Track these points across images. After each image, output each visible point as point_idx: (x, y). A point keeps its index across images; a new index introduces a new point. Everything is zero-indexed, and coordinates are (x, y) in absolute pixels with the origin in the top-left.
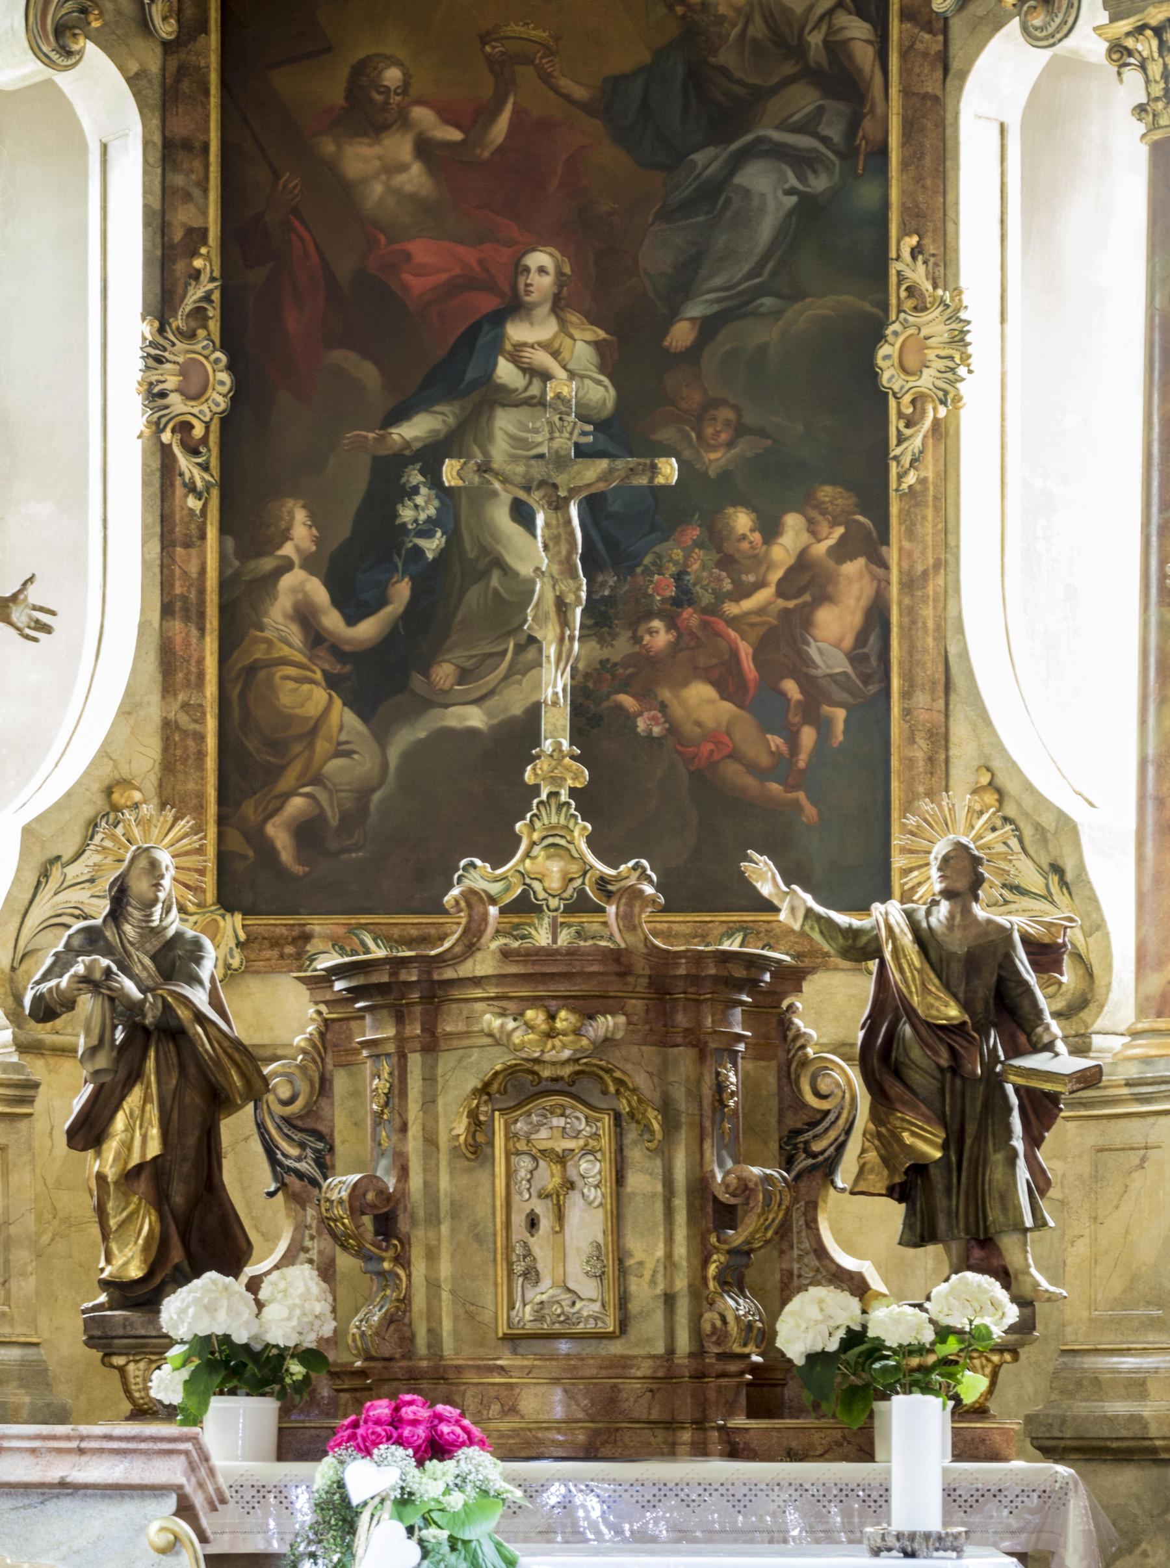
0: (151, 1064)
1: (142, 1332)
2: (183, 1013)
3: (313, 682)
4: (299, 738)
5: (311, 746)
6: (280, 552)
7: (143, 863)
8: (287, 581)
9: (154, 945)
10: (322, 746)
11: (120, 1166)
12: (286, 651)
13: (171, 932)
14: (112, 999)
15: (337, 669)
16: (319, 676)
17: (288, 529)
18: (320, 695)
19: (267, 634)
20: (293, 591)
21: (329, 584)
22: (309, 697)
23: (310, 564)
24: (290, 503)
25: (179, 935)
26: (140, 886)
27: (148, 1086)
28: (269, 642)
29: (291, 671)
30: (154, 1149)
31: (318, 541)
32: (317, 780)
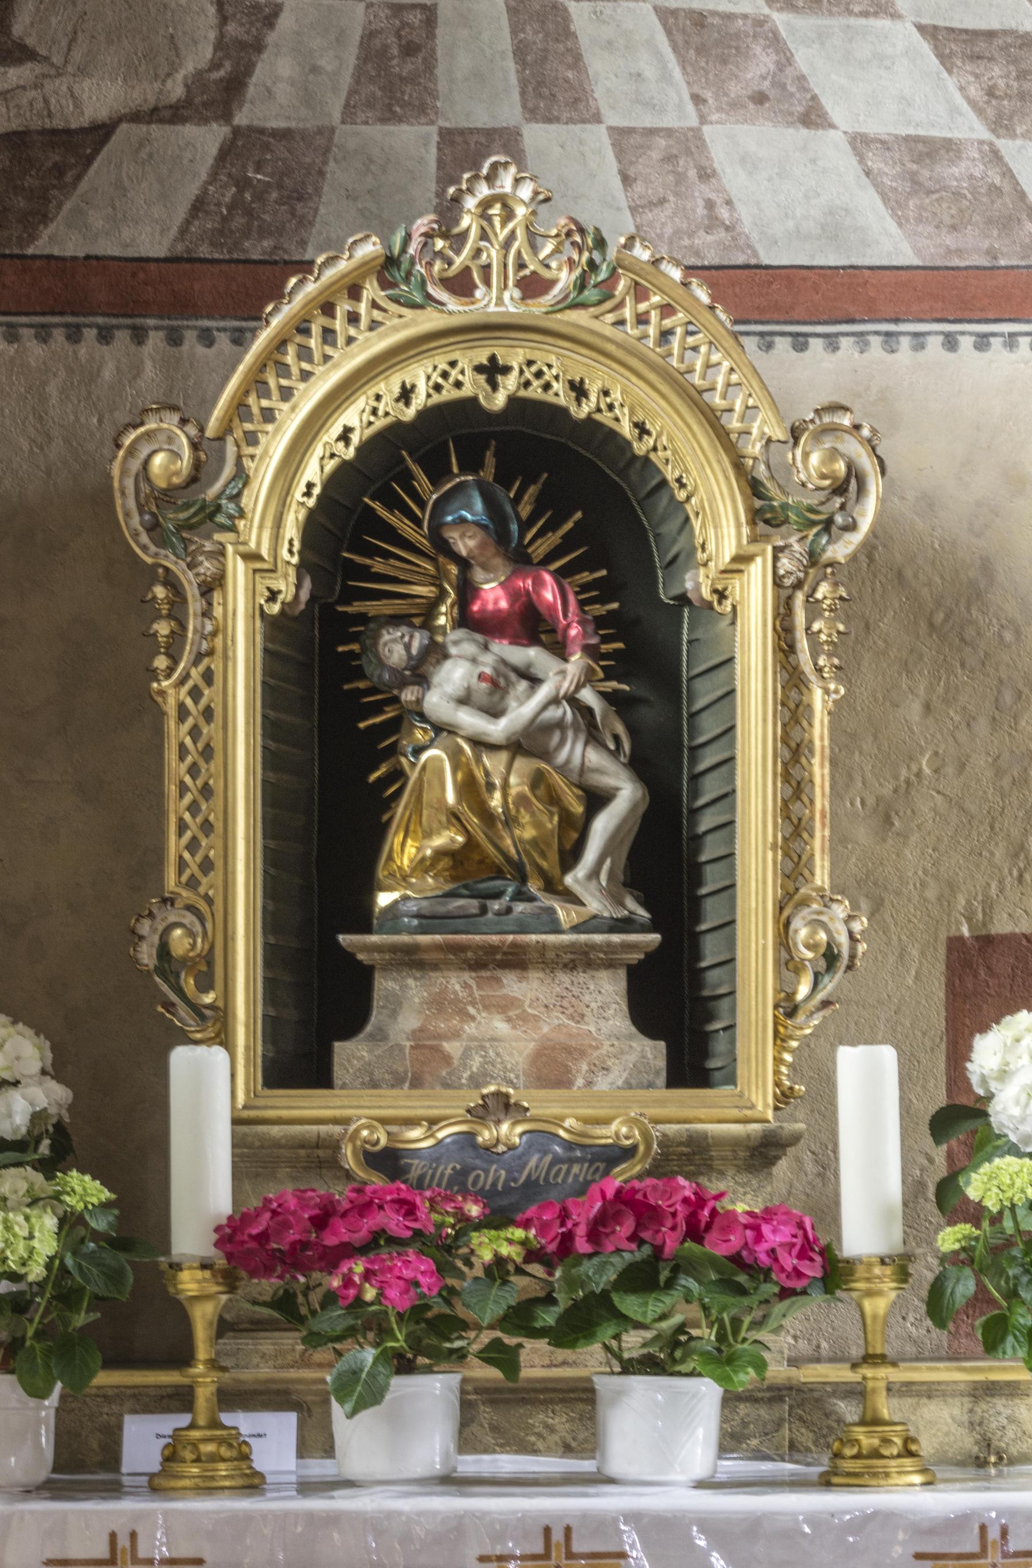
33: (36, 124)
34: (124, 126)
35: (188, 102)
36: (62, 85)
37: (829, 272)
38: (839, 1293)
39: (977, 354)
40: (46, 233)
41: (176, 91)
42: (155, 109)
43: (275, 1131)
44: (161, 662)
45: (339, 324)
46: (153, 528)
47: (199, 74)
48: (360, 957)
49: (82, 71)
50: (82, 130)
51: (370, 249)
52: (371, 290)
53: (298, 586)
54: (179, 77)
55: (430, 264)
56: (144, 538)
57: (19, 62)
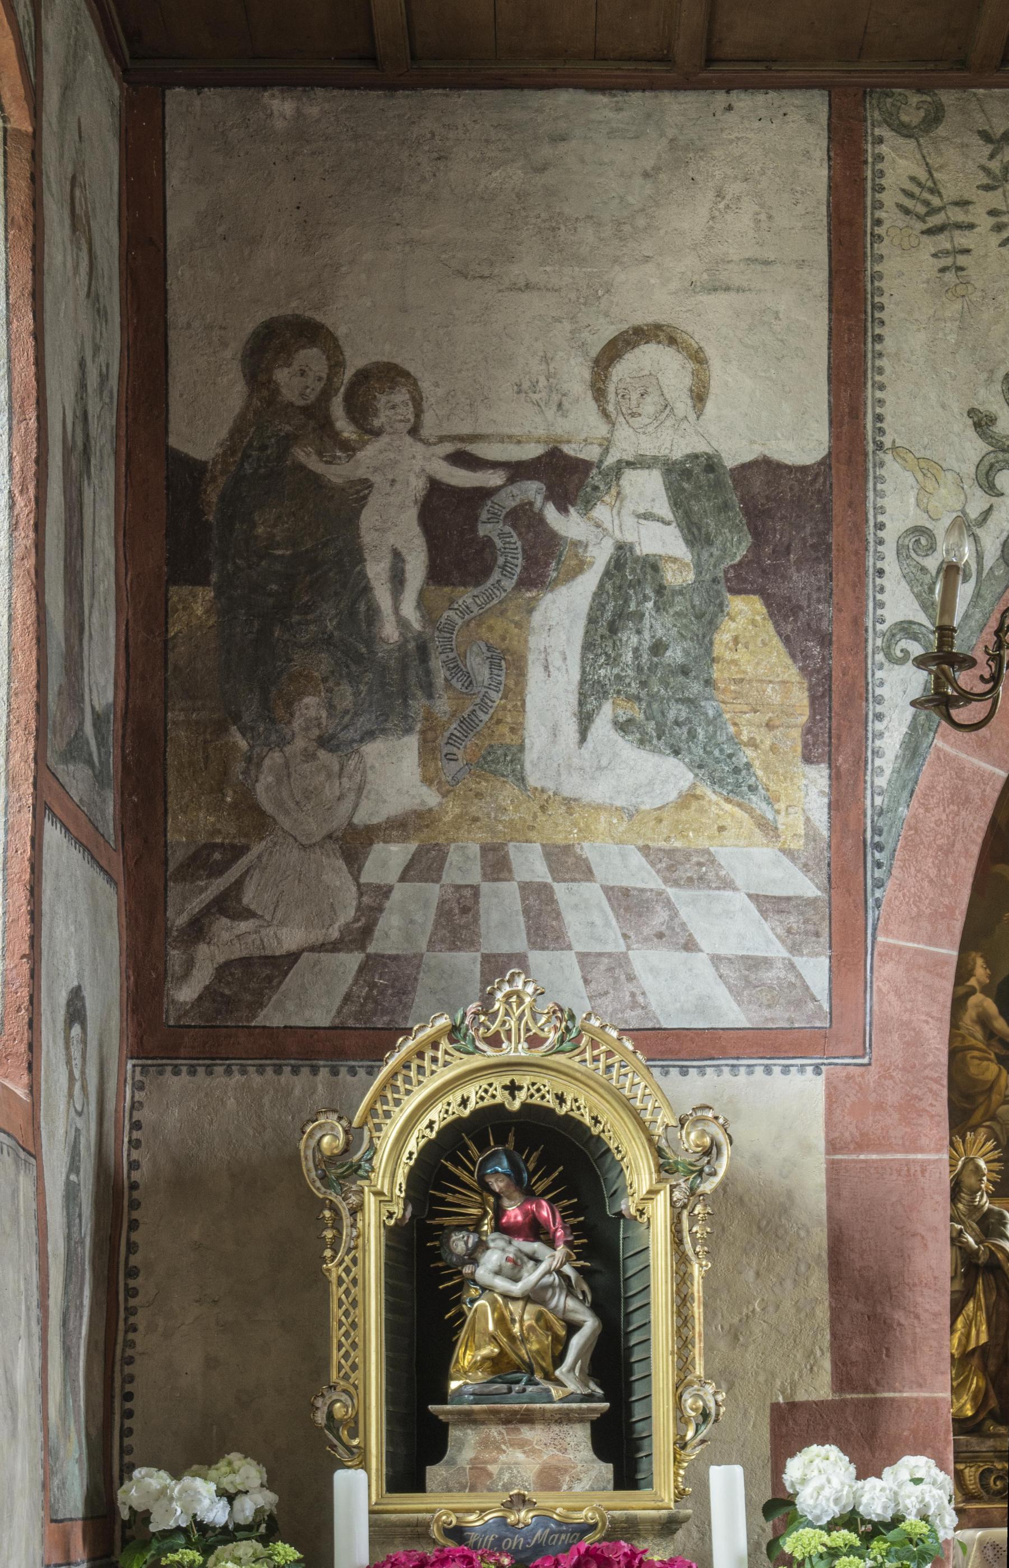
0: (980, 1287)
1: (977, 1449)
2: (1000, 1256)
3: (989, 1060)
4: (982, 1093)
5: (989, 1098)
6: (969, 983)
7: (971, 1167)
8: (973, 1000)
9: (977, 1216)
10: (996, 1098)
11: (961, 1349)
12: (973, 1042)
13: (986, 1208)
14: (960, 1248)
15: (1003, 1052)
16: (993, 1056)
17: (973, 969)
18: (994, 1068)
19: (961, 1032)
20: (977, 1006)
21: (997, 1002)
22: (987, 1069)
23: (985, 990)
24: (973, 954)
25: (990, 1210)
26: (970, 1180)
27: (979, 1300)
28: (964, 1037)
29: (976, 1053)
30: (984, 1339)
31: (990, 977)
32: (993, 1118)
33: (257, 953)
34: (305, 954)
41: (335, 934)
42: (323, 945)
44: (328, 1253)
45: (426, 1063)
46: (323, 1178)
49: (282, 924)
50: (282, 956)
52: (444, 1044)
53: (405, 1210)
54: (336, 926)
56: (318, 1184)
57: (246, 918)
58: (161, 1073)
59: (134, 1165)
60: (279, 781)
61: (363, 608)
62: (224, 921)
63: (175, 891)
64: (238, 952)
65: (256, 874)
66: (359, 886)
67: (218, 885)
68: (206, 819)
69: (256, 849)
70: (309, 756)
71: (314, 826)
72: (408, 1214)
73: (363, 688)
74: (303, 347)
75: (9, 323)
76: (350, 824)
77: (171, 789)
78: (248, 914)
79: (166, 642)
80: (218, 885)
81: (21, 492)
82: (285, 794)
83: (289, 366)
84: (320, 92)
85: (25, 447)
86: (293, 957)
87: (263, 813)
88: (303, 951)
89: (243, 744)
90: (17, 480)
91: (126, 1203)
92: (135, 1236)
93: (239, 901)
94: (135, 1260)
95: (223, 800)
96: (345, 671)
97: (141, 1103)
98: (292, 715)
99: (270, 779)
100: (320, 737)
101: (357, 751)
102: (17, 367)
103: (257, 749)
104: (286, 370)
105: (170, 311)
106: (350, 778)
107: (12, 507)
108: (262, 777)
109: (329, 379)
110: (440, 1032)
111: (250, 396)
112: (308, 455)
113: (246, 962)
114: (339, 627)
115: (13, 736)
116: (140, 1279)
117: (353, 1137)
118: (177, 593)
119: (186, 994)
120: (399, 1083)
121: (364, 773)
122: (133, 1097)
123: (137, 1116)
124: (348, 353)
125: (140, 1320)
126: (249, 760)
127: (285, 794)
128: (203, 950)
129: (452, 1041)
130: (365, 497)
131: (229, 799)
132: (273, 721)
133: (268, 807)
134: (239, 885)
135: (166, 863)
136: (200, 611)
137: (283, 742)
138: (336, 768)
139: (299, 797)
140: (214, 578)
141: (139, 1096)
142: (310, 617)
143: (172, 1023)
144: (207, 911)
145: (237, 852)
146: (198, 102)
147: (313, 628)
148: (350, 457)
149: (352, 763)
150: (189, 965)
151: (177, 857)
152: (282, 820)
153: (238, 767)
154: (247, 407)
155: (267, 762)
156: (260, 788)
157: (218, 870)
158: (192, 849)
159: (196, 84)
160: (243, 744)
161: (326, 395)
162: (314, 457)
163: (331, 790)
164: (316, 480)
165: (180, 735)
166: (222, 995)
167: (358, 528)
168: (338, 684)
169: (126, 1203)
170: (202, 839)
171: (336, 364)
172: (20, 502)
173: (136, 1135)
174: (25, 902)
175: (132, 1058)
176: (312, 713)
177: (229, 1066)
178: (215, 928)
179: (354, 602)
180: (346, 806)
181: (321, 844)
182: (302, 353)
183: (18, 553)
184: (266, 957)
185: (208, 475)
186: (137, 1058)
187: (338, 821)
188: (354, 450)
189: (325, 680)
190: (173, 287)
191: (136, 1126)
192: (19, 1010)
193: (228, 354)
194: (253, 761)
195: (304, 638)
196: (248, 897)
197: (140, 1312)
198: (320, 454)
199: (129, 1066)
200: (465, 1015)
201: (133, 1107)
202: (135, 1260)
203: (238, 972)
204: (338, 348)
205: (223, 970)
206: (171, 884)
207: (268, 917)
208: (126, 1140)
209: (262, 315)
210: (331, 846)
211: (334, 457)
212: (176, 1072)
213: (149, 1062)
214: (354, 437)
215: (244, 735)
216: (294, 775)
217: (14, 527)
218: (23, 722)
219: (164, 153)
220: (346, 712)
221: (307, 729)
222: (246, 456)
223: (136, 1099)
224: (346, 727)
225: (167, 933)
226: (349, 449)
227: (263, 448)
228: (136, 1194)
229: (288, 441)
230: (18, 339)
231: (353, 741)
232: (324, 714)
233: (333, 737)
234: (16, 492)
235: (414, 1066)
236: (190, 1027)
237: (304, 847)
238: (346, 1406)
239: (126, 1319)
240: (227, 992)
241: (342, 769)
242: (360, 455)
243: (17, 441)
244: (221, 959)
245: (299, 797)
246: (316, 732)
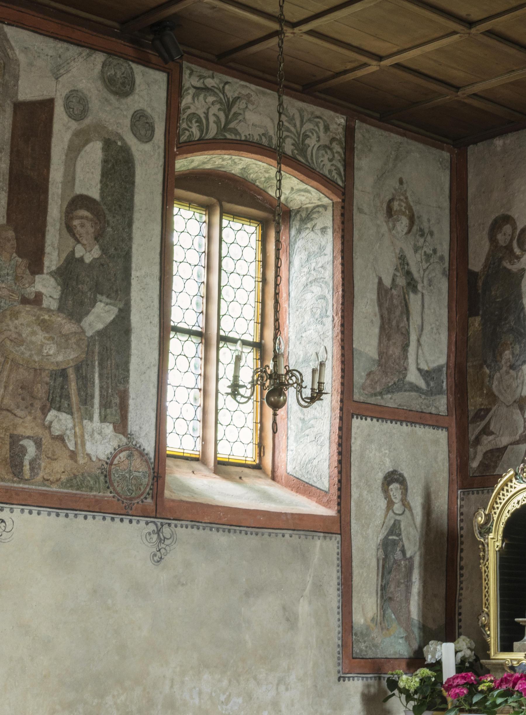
33: (494, 447)
34: (509, 446)
35: (520, 440)
36: (499, 438)
37: (33, 504)
38: (407, 688)
39: (39, 516)
40: (497, 469)
41: (518, 438)
42: (514, 442)
43: (494, 661)
44: (482, 561)
45: (509, 488)
46: (480, 533)
47: (521, 434)
48: (521, 623)
49: (502, 436)
50: (502, 448)
51: (512, 472)
52: (514, 480)
53: (502, 544)
54: (518, 435)
55: (523, 474)
56: (479, 535)
57: (491, 435)
58: (469, 494)
59: (462, 528)
60: (499, 383)
61: (522, 315)
62: (485, 437)
63: (471, 427)
64: (489, 447)
65: (494, 418)
66: (524, 419)
67: (483, 423)
68: (479, 400)
69: (494, 408)
70: (507, 373)
71: (510, 398)
72: (504, 545)
73: (522, 345)
74: (505, 225)
75: (333, 262)
76: (521, 396)
77: (469, 390)
78: (492, 433)
79: (467, 338)
80: (483, 423)
81: (336, 315)
82: (501, 387)
83: (501, 233)
84: (510, 134)
85: (338, 300)
86: (505, 448)
87: (495, 396)
88: (508, 445)
89: (488, 371)
90: (335, 312)
91: (459, 542)
92: (462, 555)
93: (489, 428)
94: (463, 563)
95: (483, 393)
96: (517, 340)
97: (463, 506)
98: (502, 359)
99: (497, 383)
100: (510, 365)
101: (521, 369)
102: (336, 275)
103: (492, 373)
104: (500, 234)
105: (469, 222)
106: (520, 379)
107: (333, 321)
108: (494, 382)
109: (512, 234)
110: (511, 476)
111: (490, 246)
112: (507, 263)
113: (491, 451)
114: (515, 324)
115: (333, 395)
116: (464, 570)
117: (488, 517)
118: (471, 319)
119: (475, 464)
120: (501, 496)
121: (523, 377)
122: (460, 503)
123: (462, 510)
124: (518, 224)
125: (464, 585)
126: (490, 377)
127: (501, 387)
128: (479, 448)
129: (516, 479)
130: (523, 275)
131: (485, 392)
132: (496, 362)
133: (496, 393)
134: (489, 423)
135: (468, 417)
136: (477, 325)
137: (500, 368)
138: (515, 376)
139: (505, 388)
140: (481, 312)
141: (463, 503)
142: (507, 322)
143: (471, 475)
144: (480, 434)
145: (488, 411)
146: (476, 148)
147: (508, 326)
148: (519, 261)
149: (520, 373)
150: (475, 453)
151: (471, 414)
152: (501, 398)
153: (487, 380)
154: (490, 249)
155: (495, 377)
156: (494, 386)
157: (483, 418)
158: (476, 411)
159: (475, 143)
160: (488, 371)
161: (511, 240)
162: (508, 263)
163: (514, 385)
164: (509, 271)
165: (470, 370)
166: (485, 464)
167: (521, 287)
168: (515, 345)
169: (459, 542)
170: (478, 407)
171: (514, 228)
172: (336, 318)
173: (462, 517)
174: (336, 449)
175: (460, 489)
176: (507, 357)
177: (488, 490)
178: (482, 439)
179: (519, 314)
180: (519, 389)
181: (512, 405)
182: (505, 227)
183: (335, 335)
184: (498, 449)
185: (479, 277)
186: (462, 489)
187: (517, 396)
188: (520, 258)
189: (511, 344)
190: (470, 214)
191: (462, 514)
192: (334, 485)
193: (484, 232)
194: (491, 377)
195: (505, 330)
196: (492, 428)
197: (464, 583)
198: (510, 262)
199: (459, 492)
200: (519, 469)
201: (460, 507)
202: (463, 563)
203: (489, 455)
204: (515, 223)
205: (485, 454)
206: (470, 425)
207: (498, 434)
208: (459, 519)
209: (493, 217)
210: (516, 405)
211: (514, 262)
212: (473, 494)
213: (465, 490)
214: (520, 253)
215: (488, 368)
216: (504, 381)
217: (334, 327)
218: (336, 390)
219: (467, 169)
220: (517, 355)
221: (506, 363)
222: (490, 267)
223: (462, 504)
224: (517, 361)
225: (469, 443)
226: (518, 258)
227: (494, 263)
228: (462, 539)
229: (501, 259)
230: (336, 267)
231: (520, 365)
232: (511, 357)
233: (514, 364)
234: (335, 316)
235: (505, 490)
236: (476, 476)
237: (507, 406)
238: (485, 619)
239: (460, 585)
240: (487, 463)
241: (517, 376)
242: (522, 260)
243: (335, 299)
244: (484, 451)
245: (505, 388)
246: (509, 364)
